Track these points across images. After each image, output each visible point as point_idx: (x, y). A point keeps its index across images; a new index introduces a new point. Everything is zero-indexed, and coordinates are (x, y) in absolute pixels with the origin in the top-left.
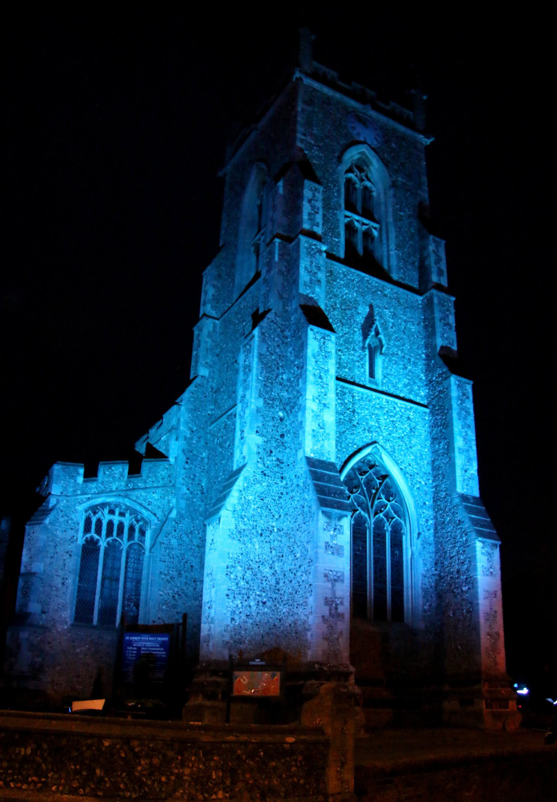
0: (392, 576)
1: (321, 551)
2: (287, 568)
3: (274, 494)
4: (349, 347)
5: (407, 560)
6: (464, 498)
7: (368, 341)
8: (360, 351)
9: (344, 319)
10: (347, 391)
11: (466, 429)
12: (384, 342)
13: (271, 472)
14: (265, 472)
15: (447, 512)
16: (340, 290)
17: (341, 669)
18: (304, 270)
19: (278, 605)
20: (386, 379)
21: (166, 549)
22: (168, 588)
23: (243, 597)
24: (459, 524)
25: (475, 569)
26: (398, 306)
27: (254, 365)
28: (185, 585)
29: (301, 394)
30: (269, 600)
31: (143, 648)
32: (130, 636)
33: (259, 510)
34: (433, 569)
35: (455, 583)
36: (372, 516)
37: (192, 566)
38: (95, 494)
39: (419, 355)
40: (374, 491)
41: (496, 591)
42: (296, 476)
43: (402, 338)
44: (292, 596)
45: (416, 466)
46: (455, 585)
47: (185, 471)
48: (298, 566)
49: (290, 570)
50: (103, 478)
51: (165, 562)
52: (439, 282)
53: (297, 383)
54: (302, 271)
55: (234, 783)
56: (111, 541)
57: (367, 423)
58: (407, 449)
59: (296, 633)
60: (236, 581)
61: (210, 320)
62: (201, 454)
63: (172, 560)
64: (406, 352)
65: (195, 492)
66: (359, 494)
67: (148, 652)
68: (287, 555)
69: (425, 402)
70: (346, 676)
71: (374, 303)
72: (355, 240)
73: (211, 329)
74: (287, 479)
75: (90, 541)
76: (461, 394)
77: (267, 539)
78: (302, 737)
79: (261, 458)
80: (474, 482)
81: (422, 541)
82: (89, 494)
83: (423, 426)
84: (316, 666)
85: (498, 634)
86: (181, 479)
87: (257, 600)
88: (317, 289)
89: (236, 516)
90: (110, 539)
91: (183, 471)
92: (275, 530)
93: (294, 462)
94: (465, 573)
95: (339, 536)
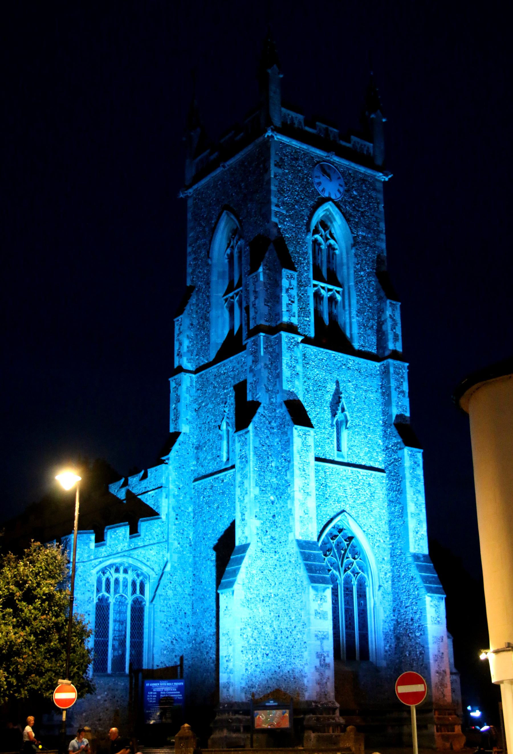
0: (359, 622)
1: (312, 617)
2: (283, 626)
4: (321, 426)
5: (370, 608)
6: (416, 557)
11: (417, 495)
16: (312, 372)
17: (330, 705)
18: (285, 366)
19: (277, 656)
20: (351, 451)
25: (425, 620)
26: (360, 377)
29: (290, 485)
30: (270, 652)
31: (162, 693)
32: (150, 683)
33: (260, 581)
34: (392, 615)
35: (410, 628)
36: (342, 572)
37: (185, 613)
38: (106, 557)
39: (377, 422)
40: (343, 552)
41: (443, 637)
42: (288, 553)
43: (363, 409)
47: (175, 527)
48: (293, 627)
49: (286, 629)
51: (164, 611)
52: (394, 348)
53: (285, 473)
58: (369, 512)
59: (294, 678)
62: (188, 509)
63: (169, 609)
64: (366, 421)
65: (185, 545)
66: (332, 556)
69: (382, 467)
70: (334, 709)
72: (321, 308)
73: (189, 385)
74: (280, 553)
75: (102, 599)
77: (267, 604)
79: (259, 538)
82: (100, 558)
84: (313, 704)
85: (445, 672)
88: (297, 383)
89: (245, 588)
91: (174, 527)
93: (286, 541)
95: (324, 604)
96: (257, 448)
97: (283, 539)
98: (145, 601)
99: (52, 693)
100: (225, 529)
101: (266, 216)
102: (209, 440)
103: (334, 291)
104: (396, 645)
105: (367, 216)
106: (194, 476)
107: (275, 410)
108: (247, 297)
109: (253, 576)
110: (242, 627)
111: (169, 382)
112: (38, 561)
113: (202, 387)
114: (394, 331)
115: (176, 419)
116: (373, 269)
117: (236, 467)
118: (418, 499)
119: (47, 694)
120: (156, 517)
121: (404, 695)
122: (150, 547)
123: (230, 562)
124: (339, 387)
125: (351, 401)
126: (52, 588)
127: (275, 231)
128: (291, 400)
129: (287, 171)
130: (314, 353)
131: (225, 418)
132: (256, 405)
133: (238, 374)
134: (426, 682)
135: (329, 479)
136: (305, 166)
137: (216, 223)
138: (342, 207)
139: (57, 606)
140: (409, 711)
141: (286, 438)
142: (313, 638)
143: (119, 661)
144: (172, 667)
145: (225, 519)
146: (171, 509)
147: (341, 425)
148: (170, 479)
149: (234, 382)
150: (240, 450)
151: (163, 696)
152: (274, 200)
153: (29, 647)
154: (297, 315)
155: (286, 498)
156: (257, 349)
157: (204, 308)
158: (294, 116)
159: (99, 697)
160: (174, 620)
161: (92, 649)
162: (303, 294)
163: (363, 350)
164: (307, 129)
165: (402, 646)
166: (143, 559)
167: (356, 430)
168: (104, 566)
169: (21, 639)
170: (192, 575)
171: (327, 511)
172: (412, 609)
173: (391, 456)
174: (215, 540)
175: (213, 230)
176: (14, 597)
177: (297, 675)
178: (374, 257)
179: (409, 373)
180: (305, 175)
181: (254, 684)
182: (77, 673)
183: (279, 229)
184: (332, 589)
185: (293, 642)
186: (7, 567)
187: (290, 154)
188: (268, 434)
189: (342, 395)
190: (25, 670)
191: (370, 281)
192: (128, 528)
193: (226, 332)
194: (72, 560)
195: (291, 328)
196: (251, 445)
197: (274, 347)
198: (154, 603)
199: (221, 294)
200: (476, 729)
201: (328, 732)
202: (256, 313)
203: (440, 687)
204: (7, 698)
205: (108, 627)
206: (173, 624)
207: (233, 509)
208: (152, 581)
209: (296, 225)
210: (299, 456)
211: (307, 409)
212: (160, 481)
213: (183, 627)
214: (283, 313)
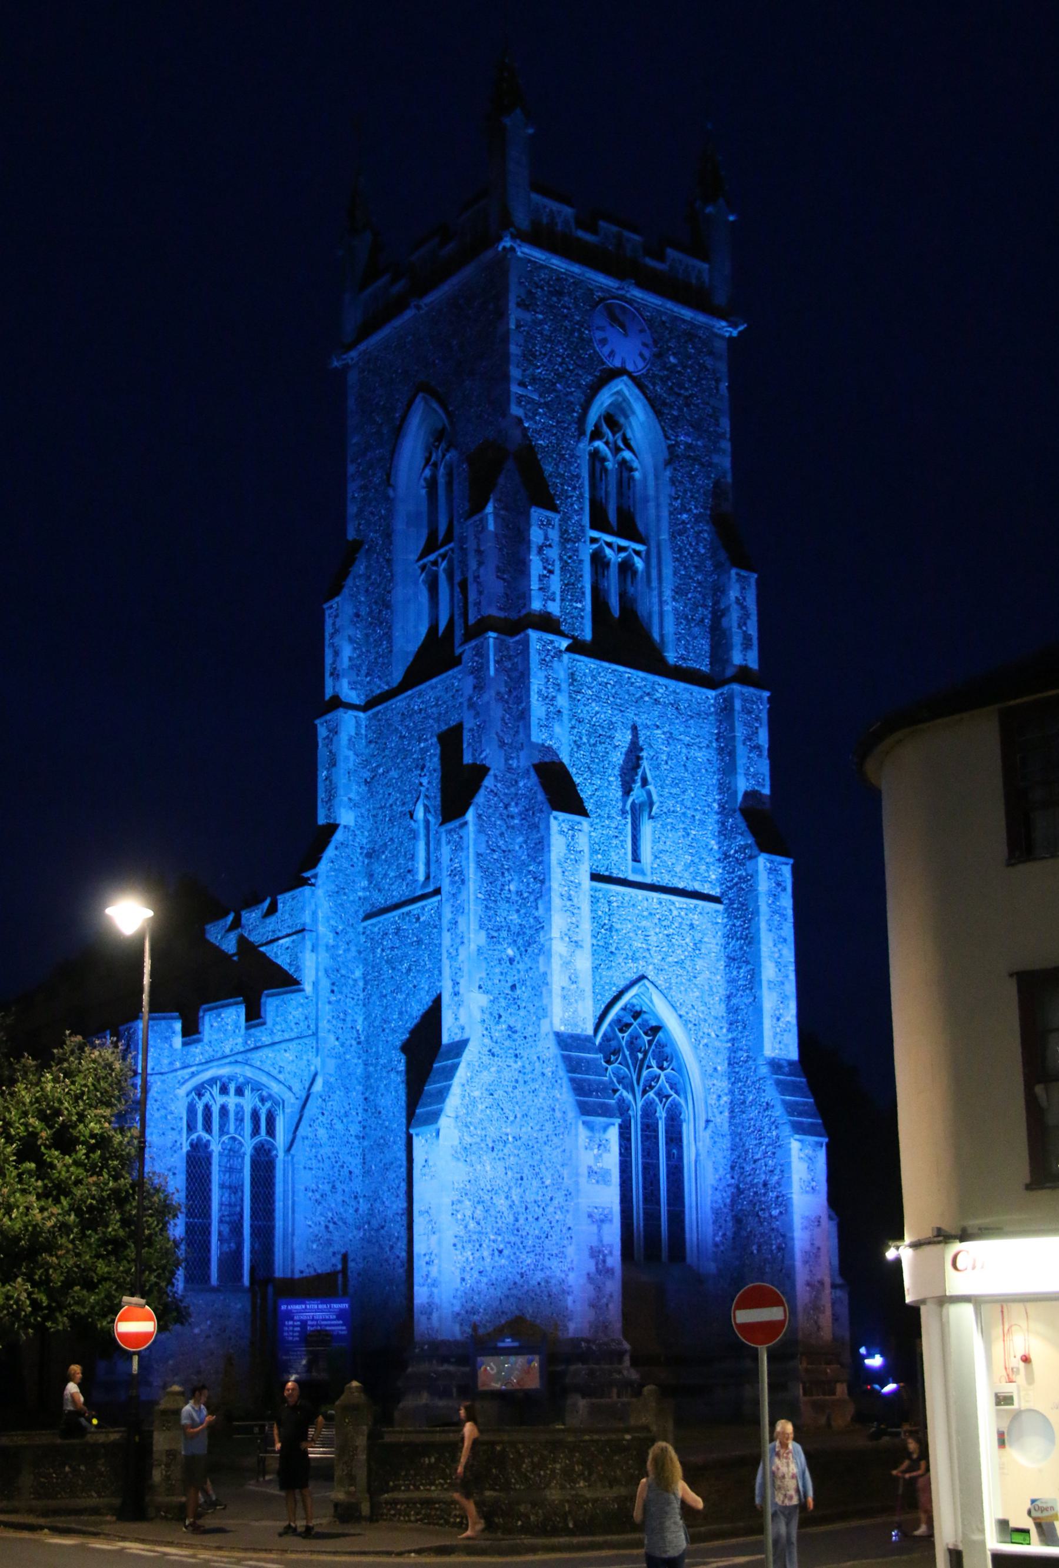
1: (583, 1180)
2: (530, 1197)
4: (602, 813)
6: (775, 1065)
8: (619, 818)
9: (593, 761)
10: (601, 896)
11: (780, 946)
12: (655, 797)
13: (501, 1049)
14: (493, 1050)
16: (587, 708)
17: (613, 1346)
18: (536, 696)
19: (518, 1253)
22: (318, 1213)
23: (474, 1246)
24: (767, 1109)
25: (789, 1184)
26: (677, 718)
28: (343, 1206)
29: (543, 927)
30: (506, 1247)
31: (309, 1323)
34: (728, 1176)
35: (760, 1202)
36: (638, 1096)
37: (350, 1173)
38: (202, 1064)
39: (709, 806)
40: (640, 1056)
42: (538, 1058)
43: (682, 780)
44: (540, 1241)
45: (702, 1008)
46: (760, 1205)
47: (330, 1007)
49: (535, 1202)
50: (210, 1035)
51: (311, 1169)
53: (534, 904)
54: (534, 698)
55: (590, 1474)
56: (226, 1141)
58: (689, 980)
59: (549, 1296)
60: (464, 1223)
61: (351, 713)
62: (353, 973)
63: (321, 1165)
65: (348, 1043)
66: (620, 1063)
67: (319, 1328)
68: (530, 1178)
69: (716, 892)
71: (639, 721)
73: (353, 733)
74: (524, 1059)
75: (197, 1145)
76: (774, 885)
77: (501, 1155)
78: (637, 1435)
79: (487, 1029)
80: (791, 1035)
81: (713, 1132)
85: (821, 1283)
86: (325, 1022)
87: (491, 1249)
88: (557, 729)
90: (225, 1138)
91: (328, 1007)
92: (511, 1139)
94: (775, 1188)
95: (605, 1155)
96: (482, 855)
98: (276, 1149)
99: (113, 1321)
101: (501, 405)
102: (391, 839)
103: (630, 550)
104: (735, 1233)
105: (697, 405)
106: (364, 908)
107: (516, 782)
108: (464, 564)
109: (474, 1101)
110: (455, 1198)
111: (315, 727)
112: (80, 1072)
113: (378, 736)
114: (744, 628)
115: (330, 800)
116: (705, 508)
117: (443, 892)
118: (781, 955)
119: (104, 1323)
121: (747, 1328)
122: (284, 1046)
123: (432, 1075)
124: (637, 738)
126: (106, 1125)
128: (546, 763)
129: (540, 316)
131: (422, 797)
132: (480, 771)
133: (447, 712)
134: (788, 1302)
135: (618, 917)
136: (577, 306)
137: (404, 418)
138: (647, 387)
139: (117, 1158)
140: (755, 1357)
141: (536, 836)
142: (585, 1220)
143: (231, 1262)
144: (328, 1274)
145: (423, 993)
146: (321, 974)
147: (641, 810)
148: (320, 915)
149: (439, 727)
150: (451, 860)
152: (515, 373)
153: (68, 1236)
154: (558, 598)
156: (482, 664)
157: (381, 583)
158: (554, 208)
159: (197, 1331)
160: (330, 1185)
161: (182, 1240)
162: (570, 557)
163: (684, 665)
164: (580, 234)
166: (271, 1069)
167: (669, 820)
168: (200, 1082)
169: (54, 1220)
170: (362, 1100)
172: (766, 1165)
173: (733, 872)
174: (403, 1033)
175: (398, 431)
176: (38, 1139)
178: (708, 485)
179: (770, 712)
180: (577, 324)
182: (157, 1284)
183: (526, 429)
184: (620, 1126)
185: (546, 1228)
186: (22, 1082)
187: (548, 283)
188: (504, 829)
189: (644, 754)
190: (62, 1278)
191: (701, 532)
192: (242, 1010)
193: (423, 630)
194: (140, 1071)
195: (548, 624)
196: (471, 850)
197: (516, 660)
198: (292, 1152)
199: (413, 557)
200: (873, 1389)
202: (480, 593)
203: (812, 1312)
204: (30, 1331)
205: (210, 1199)
206: (329, 1193)
207: (436, 972)
209: (558, 422)
210: (559, 870)
211: (577, 780)
212: (300, 919)
213: (347, 1199)
214: (533, 592)
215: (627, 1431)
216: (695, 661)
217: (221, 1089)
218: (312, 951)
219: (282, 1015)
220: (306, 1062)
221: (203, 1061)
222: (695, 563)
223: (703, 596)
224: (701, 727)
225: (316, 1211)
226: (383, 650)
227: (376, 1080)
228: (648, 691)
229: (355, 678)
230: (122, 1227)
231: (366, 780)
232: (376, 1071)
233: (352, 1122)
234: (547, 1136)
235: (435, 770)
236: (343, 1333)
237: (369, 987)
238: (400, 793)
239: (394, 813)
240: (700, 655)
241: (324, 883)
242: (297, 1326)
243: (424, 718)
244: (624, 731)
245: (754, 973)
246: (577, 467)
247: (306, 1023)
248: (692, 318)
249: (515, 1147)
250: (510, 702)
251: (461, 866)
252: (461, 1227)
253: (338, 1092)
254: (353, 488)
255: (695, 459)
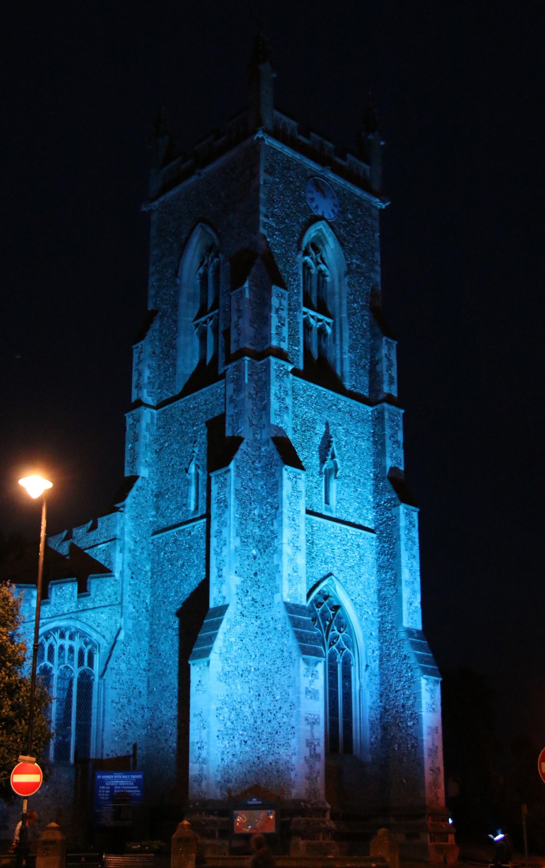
1: (302, 696)
2: (265, 707)
3: (250, 634)
6: (410, 632)
7: (325, 466)
8: (318, 477)
9: (304, 441)
11: (412, 560)
12: (339, 466)
14: (243, 613)
15: (393, 645)
16: (300, 409)
17: (320, 805)
19: (256, 744)
20: (340, 504)
21: (117, 674)
24: (405, 659)
25: (420, 706)
26: (351, 421)
27: (232, 503)
29: (277, 536)
30: (249, 739)
31: (116, 787)
32: (102, 775)
33: (239, 651)
34: (378, 701)
35: (400, 717)
36: (327, 647)
37: (140, 692)
39: (368, 475)
40: (328, 623)
41: (437, 728)
42: (272, 618)
43: (353, 458)
44: (272, 736)
45: (364, 596)
47: (131, 587)
49: (269, 710)
51: (115, 689)
52: (390, 392)
53: (270, 523)
54: (273, 398)
56: (63, 669)
57: (324, 554)
58: (357, 578)
59: (278, 771)
62: (145, 567)
63: (122, 686)
64: (357, 473)
65: (141, 610)
67: (122, 791)
68: (265, 695)
69: (372, 526)
70: (325, 811)
73: (149, 422)
74: (262, 619)
75: (43, 670)
76: (408, 523)
77: (247, 679)
79: (239, 599)
83: (371, 553)
84: (302, 804)
85: (438, 769)
86: (127, 596)
87: (240, 740)
88: (286, 418)
90: (62, 667)
91: (129, 587)
93: (270, 604)
94: (410, 708)
95: (315, 681)
97: (266, 601)
98: (94, 675)
100: (191, 590)
101: (254, 227)
102: (173, 486)
104: (382, 737)
105: (362, 244)
106: (153, 528)
107: (260, 448)
110: (219, 706)
111: (125, 418)
114: (390, 372)
116: (367, 303)
120: (109, 574)
122: (101, 610)
123: (203, 627)
125: (341, 447)
127: (263, 243)
128: (279, 437)
129: (278, 180)
130: (303, 388)
131: (194, 459)
133: (212, 408)
136: (298, 178)
137: (188, 239)
141: (273, 481)
142: (304, 722)
145: (192, 579)
146: (126, 566)
148: (126, 530)
149: (207, 417)
150: (218, 493)
151: (117, 792)
152: (263, 209)
155: (272, 551)
156: (240, 376)
157: (169, 334)
163: (355, 391)
164: (301, 138)
165: (389, 737)
166: (92, 624)
167: (346, 481)
170: (148, 647)
171: (313, 573)
172: (404, 694)
173: (383, 515)
174: (178, 604)
175: (184, 247)
177: (281, 768)
178: (368, 289)
181: (231, 778)
183: (268, 242)
185: (276, 727)
188: (252, 475)
191: (364, 316)
193: (196, 362)
195: (281, 354)
197: (260, 375)
198: (104, 677)
199: (191, 319)
201: (318, 839)
203: (433, 788)
206: (126, 705)
208: (103, 651)
209: (286, 241)
210: (288, 502)
213: (137, 709)
214: (273, 335)
215: (372, 860)
216: (361, 389)
217: (60, 635)
218: (120, 552)
219: (101, 590)
220: (114, 621)
221: (50, 616)
222: (361, 333)
223: (365, 352)
224: (364, 428)
225: (118, 716)
226: (170, 373)
227: (158, 634)
228: (335, 403)
229: (151, 390)
230: (11, 710)
231: (156, 451)
232: (159, 628)
233: (142, 660)
234: (278, 668)
235: (203, 443)
236: (139, 794)
237: (155, 576)
238: (179, 458)
239: (175, 470)
240: (363, 386)
241: (129, 511)
242: (107, 790)
243: (196, 412)
244: (321, 425)
245: (396, 575)
246: (296, 268)
247: (115, 596)
248: (360, 194)
249: (255, 675)
250: (257, 400)
251: (225, 497)
252: (222, 725)
253: (134, 641)
254: (152, 280)
255: (362, 274)
